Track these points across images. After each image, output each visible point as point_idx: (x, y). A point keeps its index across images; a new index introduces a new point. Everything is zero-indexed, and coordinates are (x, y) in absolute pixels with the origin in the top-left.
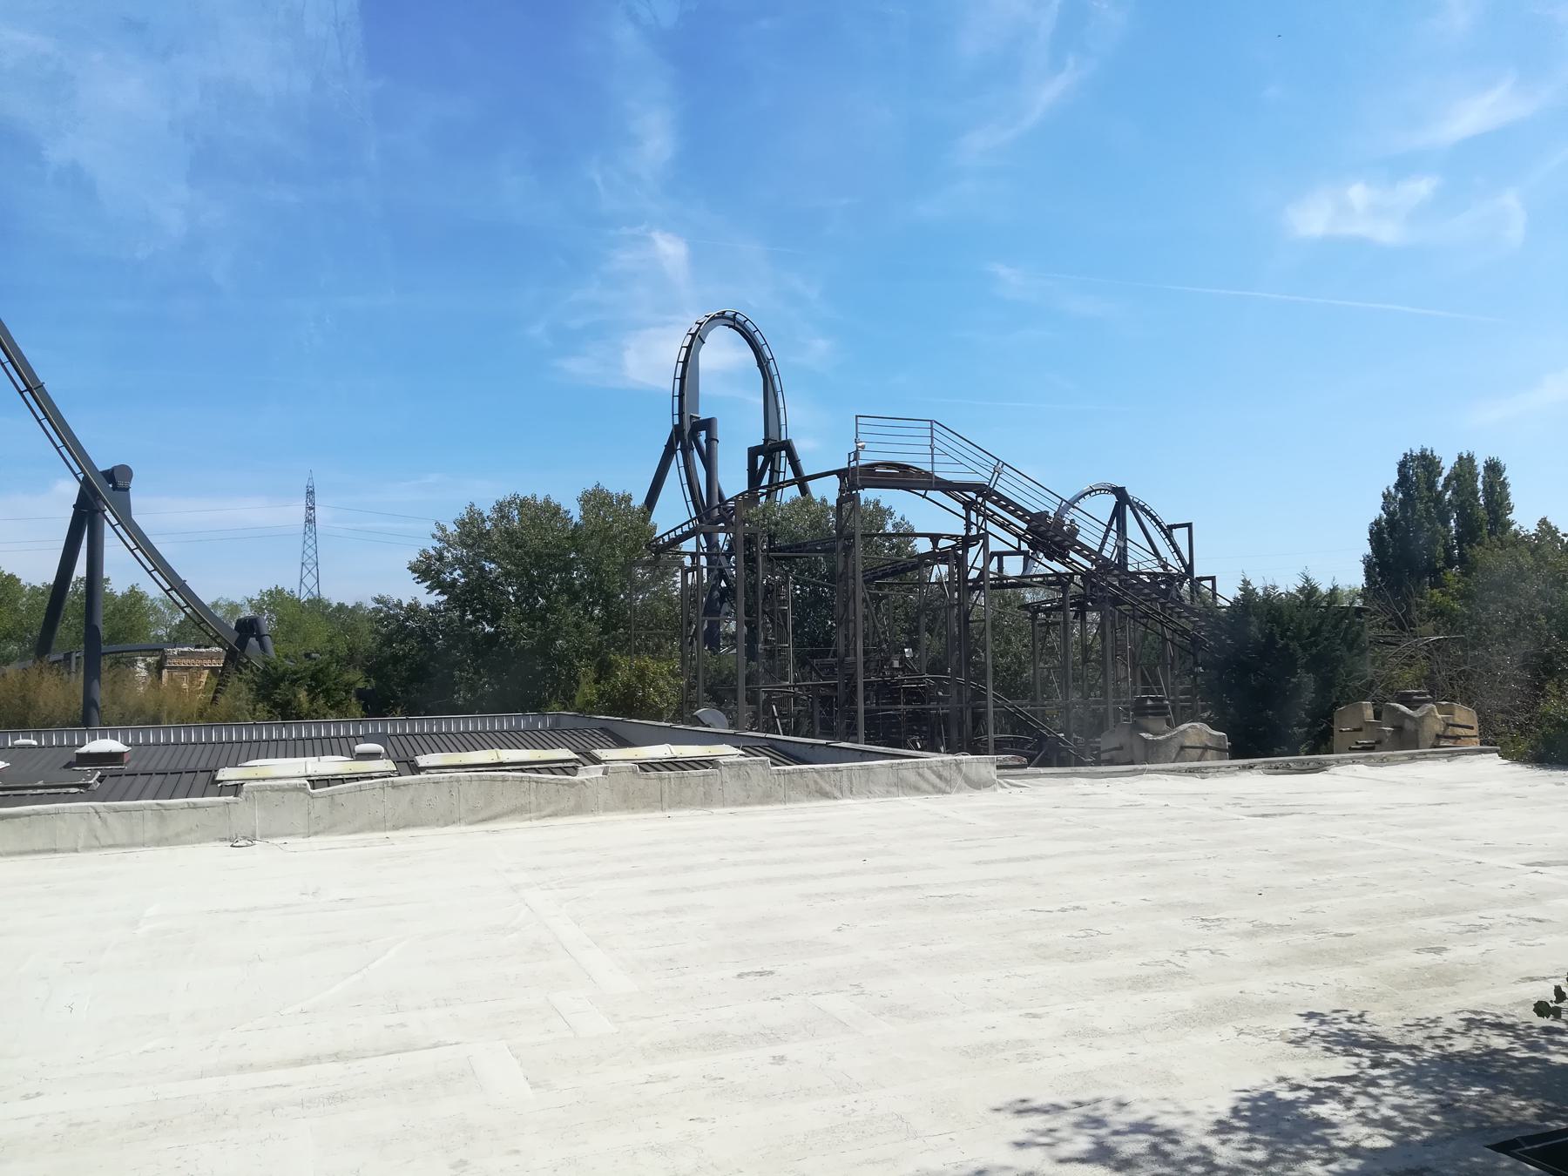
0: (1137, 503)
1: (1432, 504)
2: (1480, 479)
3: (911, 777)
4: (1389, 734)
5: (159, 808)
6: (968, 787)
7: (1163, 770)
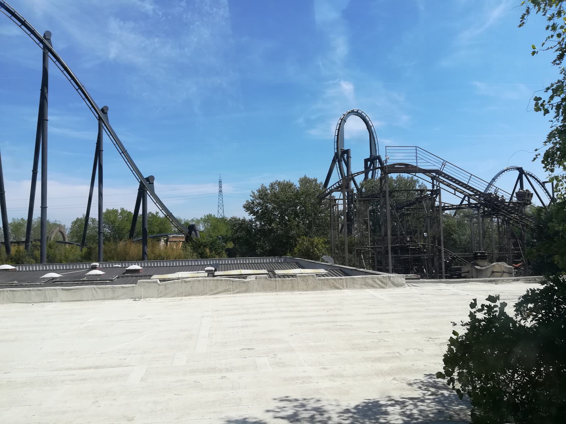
0: (528, 174)
6: (393, 286)
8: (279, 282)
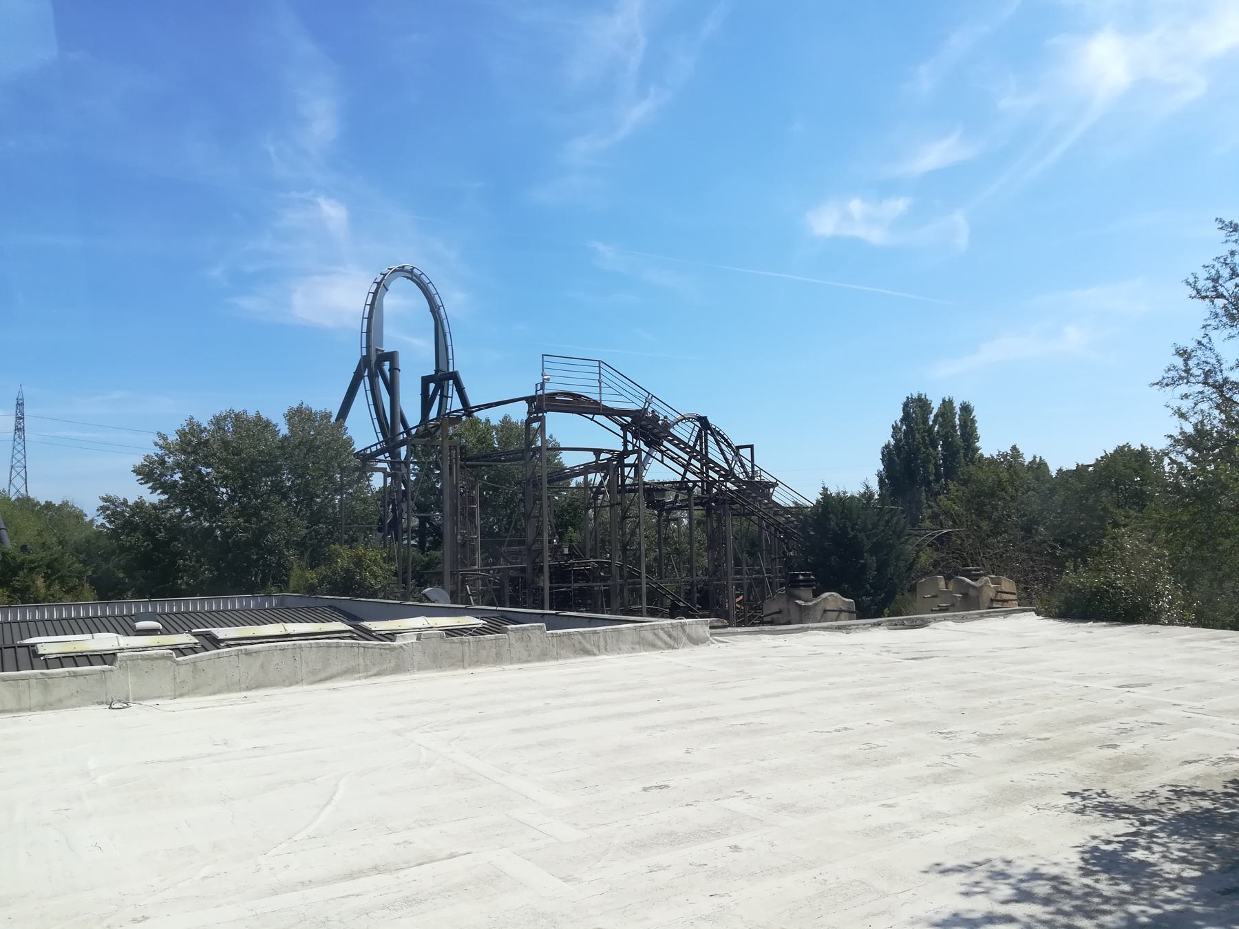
0: (715, 429)
1: (927, 434)
2: (957, 416)
3: (650, 636)
4: (959, 599)
5: (43, 677)
7: (821, 628)
8: (470, 645)
